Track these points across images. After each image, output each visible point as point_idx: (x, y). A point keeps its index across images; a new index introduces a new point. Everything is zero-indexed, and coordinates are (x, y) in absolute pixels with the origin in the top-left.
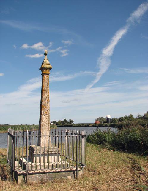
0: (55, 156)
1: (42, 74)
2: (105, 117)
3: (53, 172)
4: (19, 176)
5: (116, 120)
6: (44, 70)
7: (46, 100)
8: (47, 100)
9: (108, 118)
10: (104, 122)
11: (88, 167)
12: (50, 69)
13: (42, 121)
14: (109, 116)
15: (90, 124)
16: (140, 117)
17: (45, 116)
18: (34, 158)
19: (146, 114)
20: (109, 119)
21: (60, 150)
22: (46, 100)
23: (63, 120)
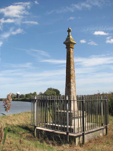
0: (76, 119)
1: (66, 48)
2: (15, 93)
3: (97, 130)
4: (76, 138)
5: (24, 96)
6: (71, 45)
7: (73, 70)
8: (74, 71)
9: (17, 95)
10: (15, 98)
11: (18, 133)
12: (75, 44)
13: (72, 89)
14: (19, 93)
15: (3, 99)
16: (41, 94)
17: (73, 84)
18: (73, 120)
19: (52, 89)
20: (19, 95)
21: (77, 115)
22: (73, 70)
23: (32, 93)
